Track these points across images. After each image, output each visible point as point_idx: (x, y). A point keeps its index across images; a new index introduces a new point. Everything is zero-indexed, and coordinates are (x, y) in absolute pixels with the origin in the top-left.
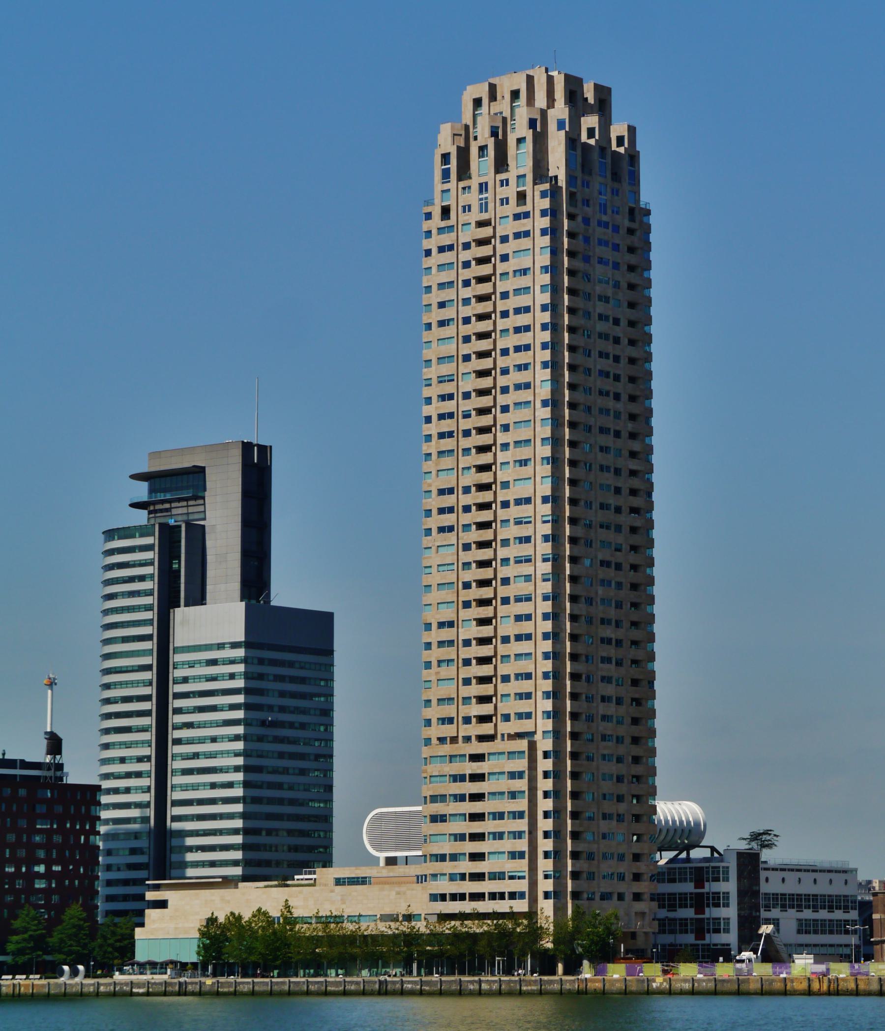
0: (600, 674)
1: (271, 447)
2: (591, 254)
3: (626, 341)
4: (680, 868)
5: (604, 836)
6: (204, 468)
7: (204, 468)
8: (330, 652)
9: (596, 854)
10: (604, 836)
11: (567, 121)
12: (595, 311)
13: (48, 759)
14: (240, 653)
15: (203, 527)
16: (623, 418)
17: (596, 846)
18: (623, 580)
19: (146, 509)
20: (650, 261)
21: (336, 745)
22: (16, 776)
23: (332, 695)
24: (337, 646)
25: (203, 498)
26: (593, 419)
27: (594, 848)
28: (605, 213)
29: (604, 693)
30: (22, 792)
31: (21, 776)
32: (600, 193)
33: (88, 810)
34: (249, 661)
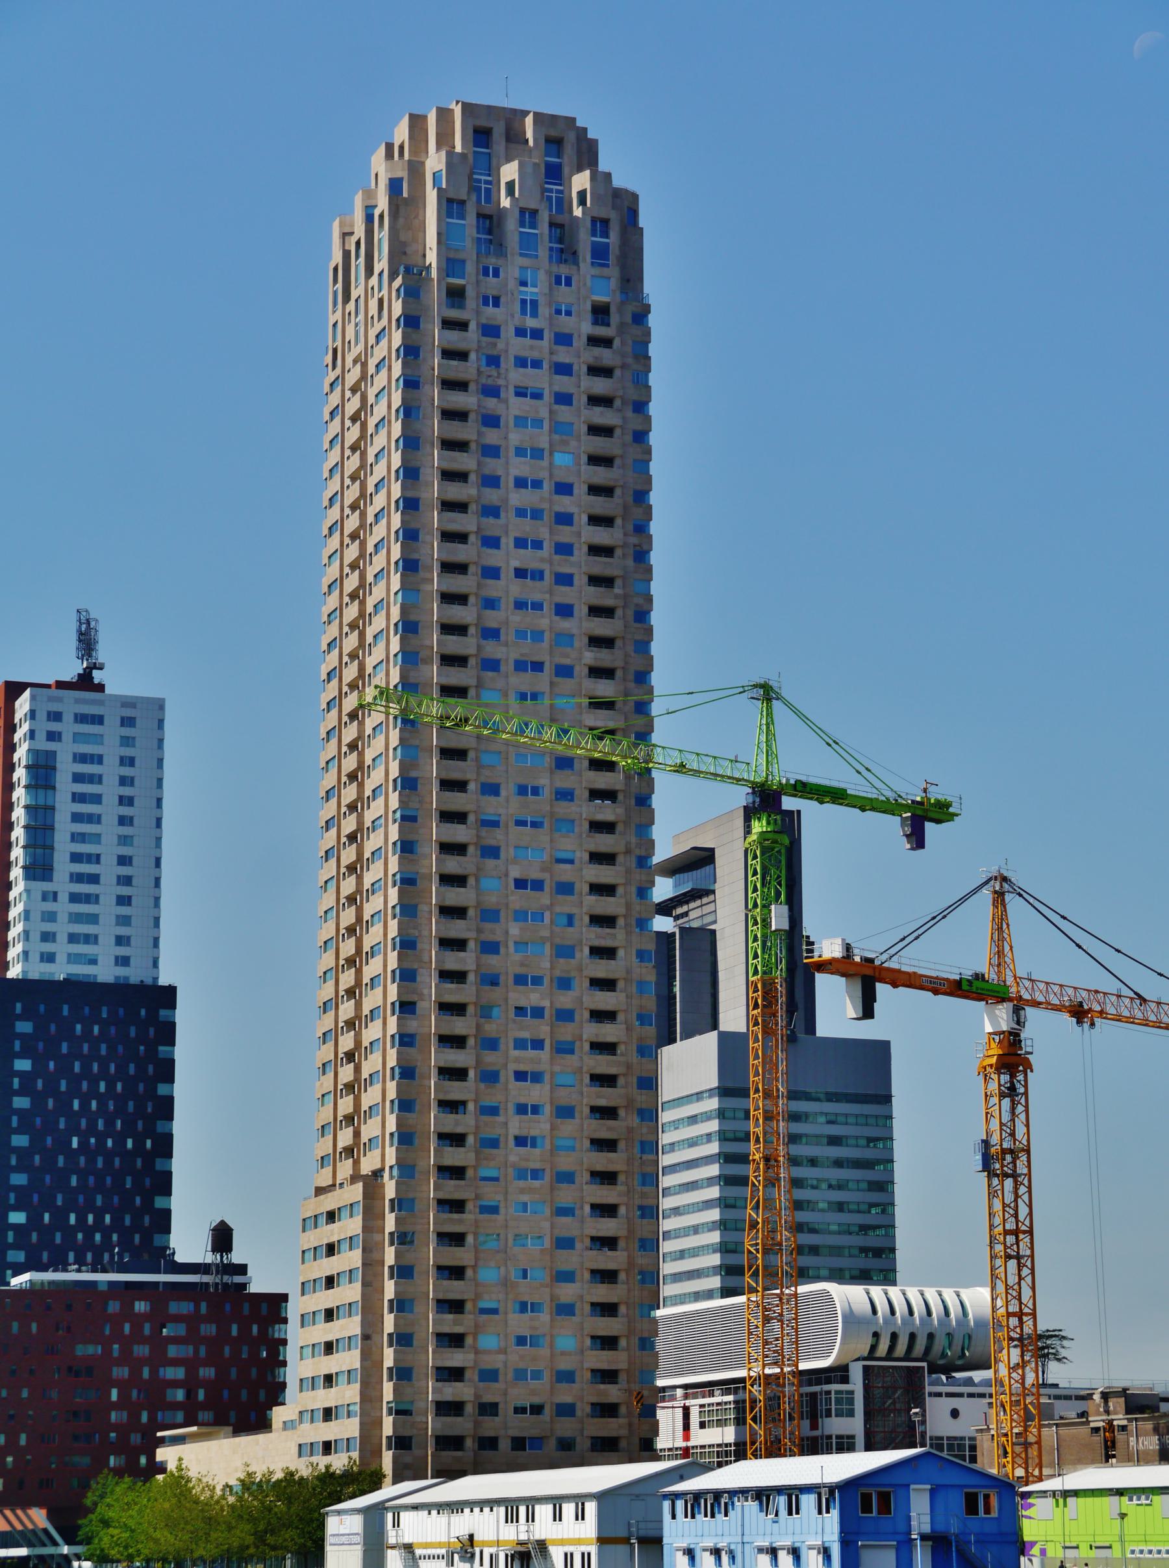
0: (513, 1067)
1: (799, 812)
2: (501, 382)
3: (585, 518)
4: (837, 1392)
5: (521, 1341)
6: (712, 850)
7: (712, 850)
8: (887, 1099)
9: (501, 1372)
10: (521, 1341)
11: (444, 172)
12: (508, 474)
13: (209, 1258)
14: (713, 1104)
15: (714, 932)
16: (577, 644)
17: (501, 1357)
18: (574, 910)
19: (670, 915)
20: (650, 387)
21: (900, 1233)
22: (158, 1283)
23: (892, 1161)
24: (895, 1090)
25: (713, 892)
26: (504, 649)
27: (497, 1362)
28: (535, 314)
29: (523, 1100)
30: (140, 1306)
31: (165, 1283)
32: (524, 283)
33: (263, 1332)
34: (728, 1114)
